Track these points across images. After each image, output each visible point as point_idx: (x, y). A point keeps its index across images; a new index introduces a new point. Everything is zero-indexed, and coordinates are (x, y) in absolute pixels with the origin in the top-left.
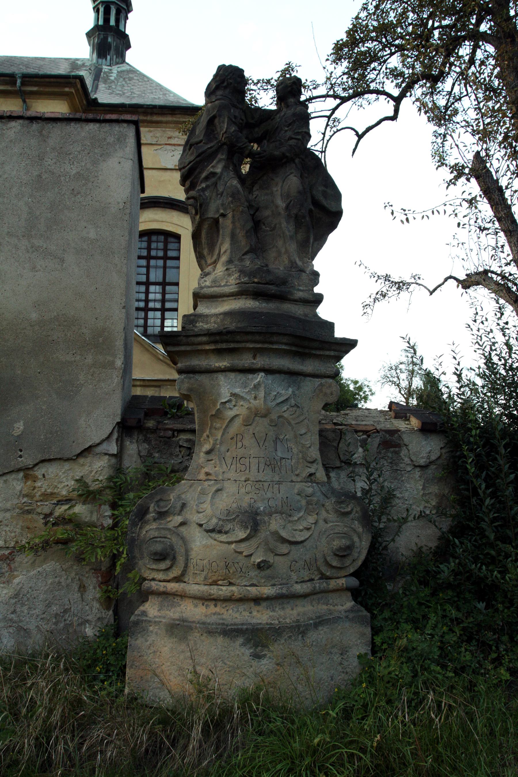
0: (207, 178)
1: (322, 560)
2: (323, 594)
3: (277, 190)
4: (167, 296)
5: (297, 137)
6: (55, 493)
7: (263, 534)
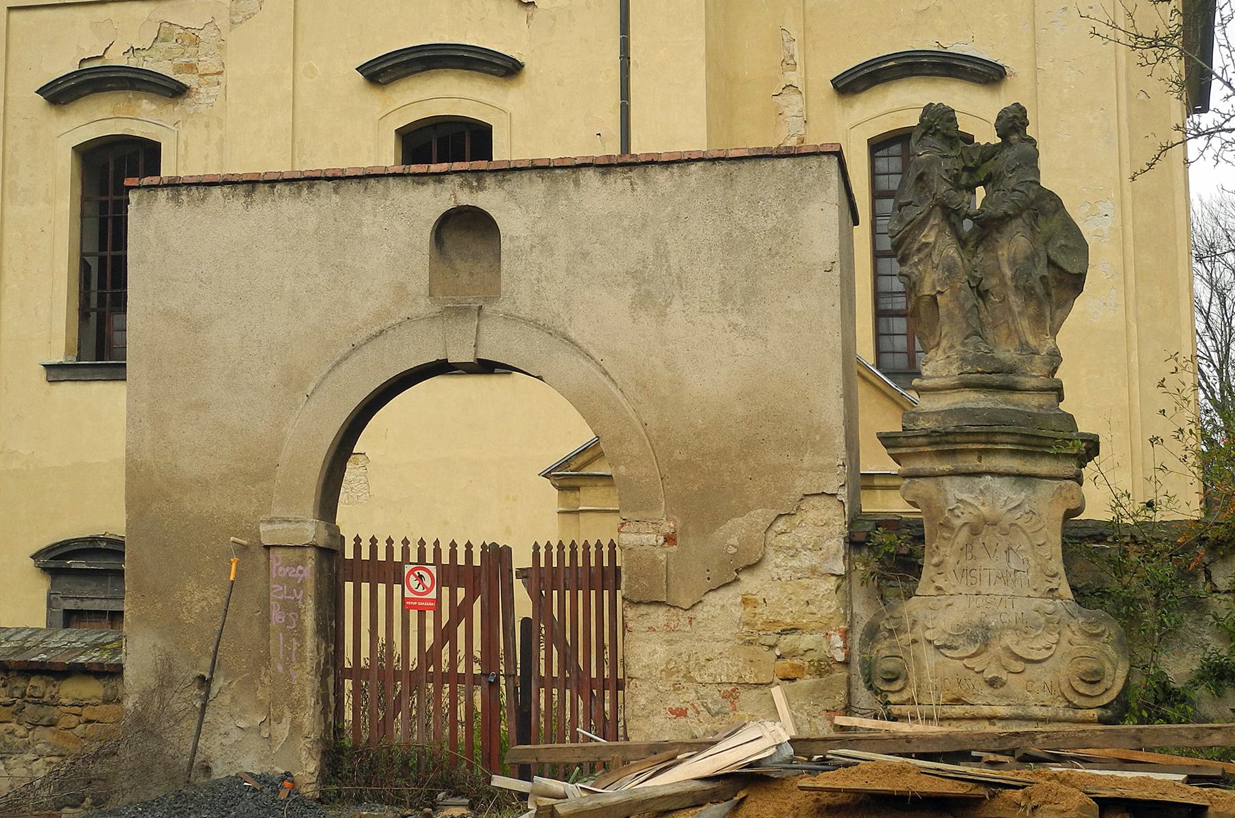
0: (919, 250)
5: (1021, 188)
7: (996, 649)
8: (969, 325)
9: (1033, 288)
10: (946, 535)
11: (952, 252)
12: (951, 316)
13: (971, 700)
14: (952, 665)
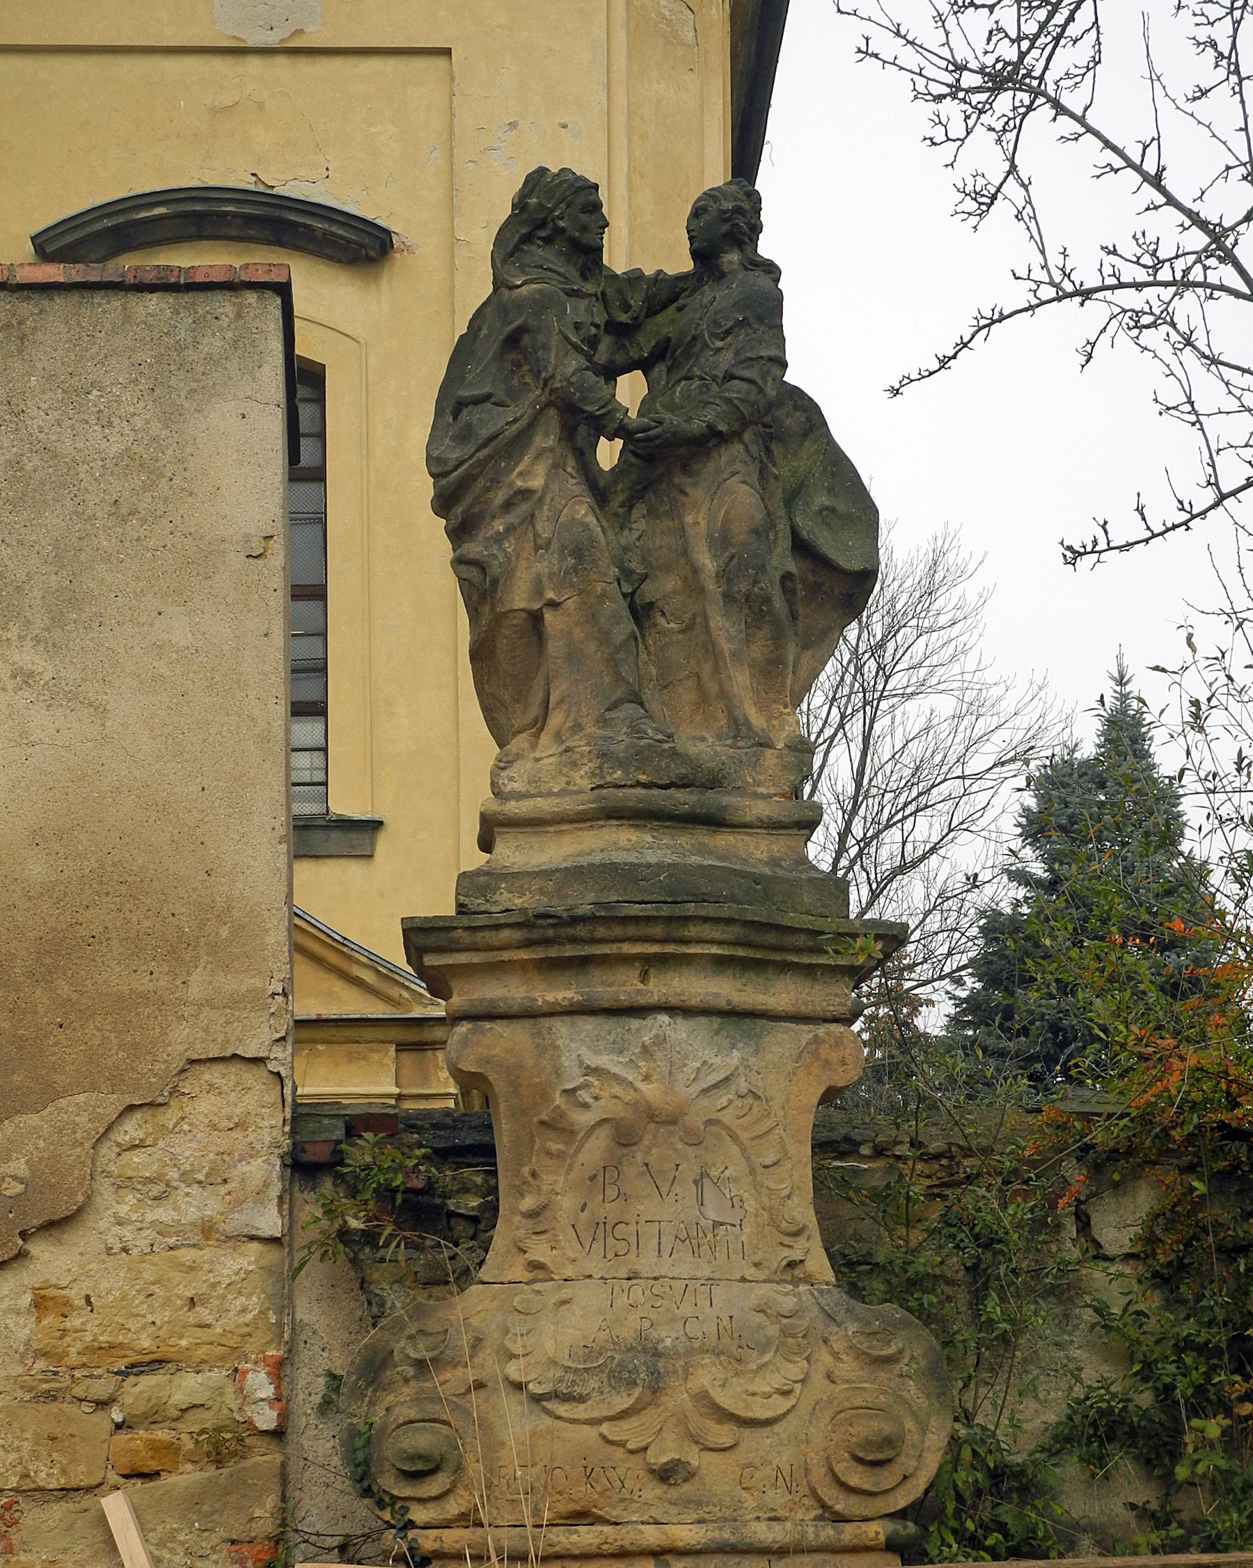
0: (508, 505)
1: (824, 1470)
2: (828, 1557)
5: (747, 374)
6: (121, 1344)
7: (678, 1398)
8: (619, 678)
9: (767, 600)
10: (554, 1147)
11: (583, 511)
12: (574, 657)
13: (614, 1514)
14: (573, 1436)
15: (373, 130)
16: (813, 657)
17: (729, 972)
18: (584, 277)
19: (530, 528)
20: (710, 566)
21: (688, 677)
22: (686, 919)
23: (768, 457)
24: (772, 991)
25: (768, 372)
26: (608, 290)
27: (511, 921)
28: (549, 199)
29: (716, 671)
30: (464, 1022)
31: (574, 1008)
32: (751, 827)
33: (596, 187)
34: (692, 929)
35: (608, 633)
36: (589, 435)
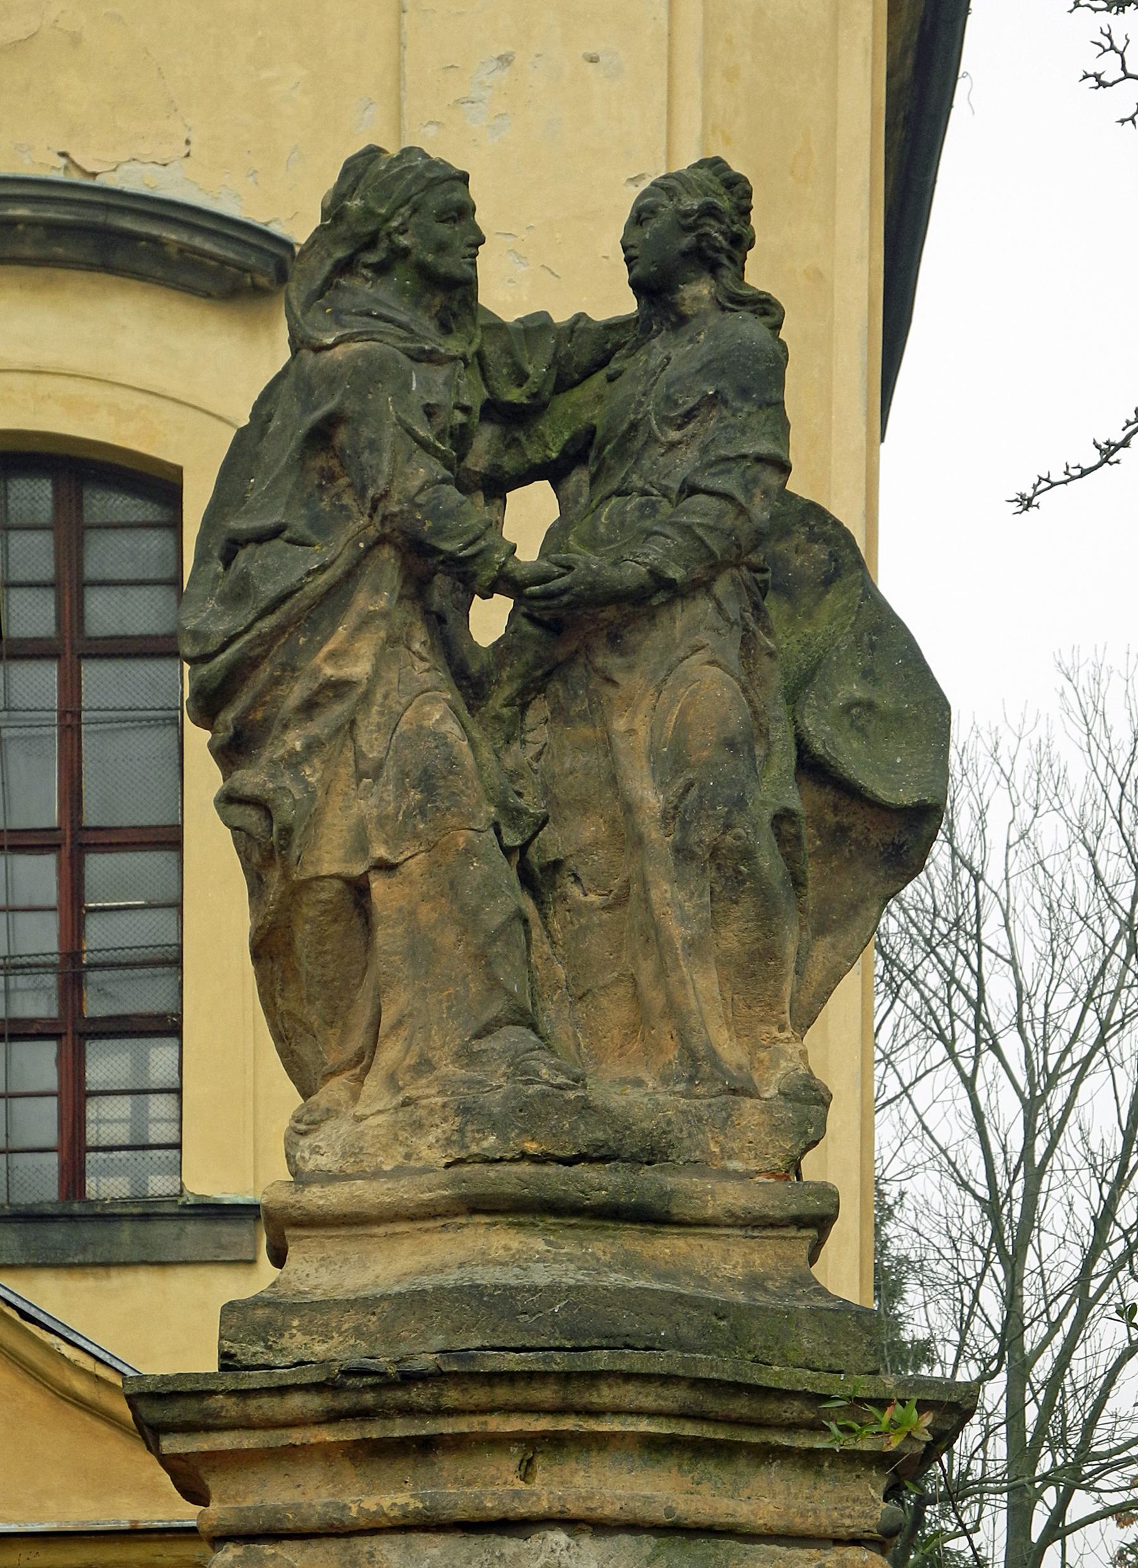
0: (309, 707)
3: (631, 732)
4: (99, 935)
8: (494, 984)
9: (747, 855)
11: (439, 714)
12: (420, 951)
15: (265, 74)
16: (834, 946)
17: (672, 1462)
18: (446, 329)
19: (349, 743)
20: (653, 801)
21: (617, 981)
22: (595, 1377)
23: (757, 620)
24: (747, 1492)
25: (755, 481)
26: (489, 349)
27: (306, 1380)
28: (381, 202)
29: (662, 972)
30: (230, 1546)
31: (410, 1521)
32: (717, 1226)
33: (464, 178)
34: (605, 1391)
35: (476, 912)
36: (454, 589)
